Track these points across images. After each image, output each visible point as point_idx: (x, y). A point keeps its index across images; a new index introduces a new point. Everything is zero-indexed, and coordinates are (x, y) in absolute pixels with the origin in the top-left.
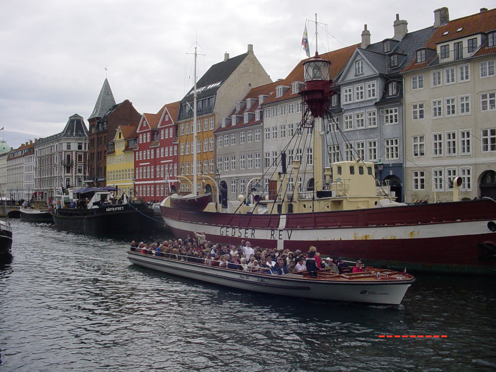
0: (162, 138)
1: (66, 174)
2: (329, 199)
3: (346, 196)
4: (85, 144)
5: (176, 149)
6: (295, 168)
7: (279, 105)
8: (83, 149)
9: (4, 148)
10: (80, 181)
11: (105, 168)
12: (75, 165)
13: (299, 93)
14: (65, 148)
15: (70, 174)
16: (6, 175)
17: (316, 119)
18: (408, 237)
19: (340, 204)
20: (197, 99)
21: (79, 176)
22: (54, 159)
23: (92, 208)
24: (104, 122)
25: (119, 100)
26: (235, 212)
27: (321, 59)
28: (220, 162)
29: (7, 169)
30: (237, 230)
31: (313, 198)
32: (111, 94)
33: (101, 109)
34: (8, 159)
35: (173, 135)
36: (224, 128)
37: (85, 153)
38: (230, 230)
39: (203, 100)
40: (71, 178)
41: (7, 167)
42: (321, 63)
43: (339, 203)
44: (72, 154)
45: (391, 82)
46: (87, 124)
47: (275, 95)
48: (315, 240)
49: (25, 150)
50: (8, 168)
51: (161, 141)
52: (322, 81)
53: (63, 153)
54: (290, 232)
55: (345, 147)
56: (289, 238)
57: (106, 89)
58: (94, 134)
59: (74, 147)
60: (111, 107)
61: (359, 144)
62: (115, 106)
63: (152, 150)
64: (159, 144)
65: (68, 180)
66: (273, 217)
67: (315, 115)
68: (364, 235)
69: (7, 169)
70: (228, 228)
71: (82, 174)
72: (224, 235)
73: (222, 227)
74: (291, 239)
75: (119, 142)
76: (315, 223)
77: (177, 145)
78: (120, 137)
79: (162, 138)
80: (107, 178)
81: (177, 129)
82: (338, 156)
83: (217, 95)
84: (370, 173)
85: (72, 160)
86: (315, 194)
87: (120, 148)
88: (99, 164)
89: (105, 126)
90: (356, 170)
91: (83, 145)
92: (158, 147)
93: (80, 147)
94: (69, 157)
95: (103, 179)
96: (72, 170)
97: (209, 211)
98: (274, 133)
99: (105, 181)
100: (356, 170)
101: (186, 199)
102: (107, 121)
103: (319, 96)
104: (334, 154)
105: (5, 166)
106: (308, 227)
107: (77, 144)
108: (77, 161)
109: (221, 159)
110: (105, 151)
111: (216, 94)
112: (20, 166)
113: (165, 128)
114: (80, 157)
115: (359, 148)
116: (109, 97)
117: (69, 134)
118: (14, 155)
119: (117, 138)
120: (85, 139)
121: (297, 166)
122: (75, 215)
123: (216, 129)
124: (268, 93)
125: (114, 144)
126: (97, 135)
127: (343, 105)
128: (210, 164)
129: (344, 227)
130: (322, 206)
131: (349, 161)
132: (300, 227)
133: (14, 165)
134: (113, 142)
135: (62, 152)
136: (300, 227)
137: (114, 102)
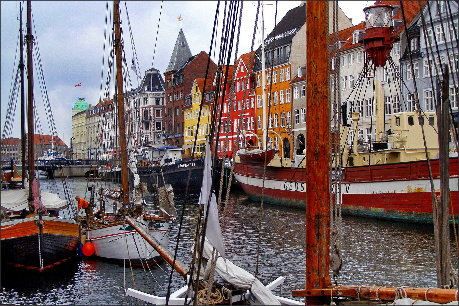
0: (239, 91)
1: (156, 130)
2: (384, 151)
3: (404, 147)
4: (163, 98)
5: (252, 101)
6: (354, 120)
7: (355, 52)
8: (161, 104)
9: (83, 106)
10: (158, 138)
11: (183, 123)
12: (153, 121)
13: (359, 42)
14: (142, 103)
15: (148, 131)
16: (85, 133)
17: (378, 69)
18: (405, 191)
19: (397, 156)
20: (265, 51)
21: (157, 132)
22: (132, 116)
23: (164, 165)
24: (180, 75)
25: (195, 52)
26: (298, 166)
27: (382, 4)
28: (297, 115)
29: (86, 127)
30: (300, 184)
31: (370, 151)
32: (187, 46)
33: (177, 62)
34: (87, 117)
35: (250, 88)
36: (300, 78)
37: (163, 108)
38: (293, 184)
39: (278, 49)
40: (149, 134)
41: (86, 125)
42: (382, 8)
43: (396, 155)
44: (150, 110)
45: (412, 38)
46: (164, 78)
47: (352, 40)
48: (370, 193)
49: (103, 107)
50: (87, 126)
51: (238, 94)
52: (383, 28)
53: (141, 109)
54: (348, 185)
55: (425, 94)
56: (347, 192)
57: (181, 41)
58: (170, 89)
59: (151, 102)
60: (187, 59)
61: (428, 92)
62: (192, 58)
63: (252, 99)
64: (236, 97)
65: (147, 136)
66: (372, 168)
67: (376, 64)
68: (417, 188)
69: (86, 127)
70: (291, 182)
71: (161, 130)
72: (288, 189)
73: (286, 182)
74: (349, 193)
75: (195, 96)
76: (371, 176)
77: (254, 97)
78: (196, 91)
79: (239, 91)
80: (185, 133)
81: (253, 81)
82: (399, 108)
83: (293, 44)
84: (432, 123)
85: (150, 116)
86: (372, 146)
87: (196, 101)
88: (177, 119)
89: (181, 80)
90: (416, 120)
91: (161, 100)
92: (235, 101)
93: (157, 102)
94: (146, 113)
95: (181, 135)
96: (150, 126)
97: (274, 166)
98: (351, 82)
99: (183, 137)
100: (416, 120)
101: (250, 153)
102: (183, 74)
103: (379, 44)
104: (414, 102)
105: (83, 124)
106: (387, 179)
107: (155, 99)
108: (156, 117)
109: (298, 111)
110: (182, 106)
111: (291, 42)
112: (90, 125)
113: (241, 80)
114: (158, 112)
115: (428, 97)
116: (185, 49)
117: (146, 89)
118: (92, 113)
119: (193, 91)
120: (163, 94)
121: (356, 118)
122: (148, 173)
123: (292, 80)
124: (345, 39)
125: (191, 98)
126: (174, 89)
127: (423, 49)
128: (287, 117)
129: (398, 179)
130: (378, 159)
131: (409, 112)
132: (357, 181)
133: (91, 124)
134: (189, 96)
135: (139, 108)
136: (357, 181)
137: (190, 54)
